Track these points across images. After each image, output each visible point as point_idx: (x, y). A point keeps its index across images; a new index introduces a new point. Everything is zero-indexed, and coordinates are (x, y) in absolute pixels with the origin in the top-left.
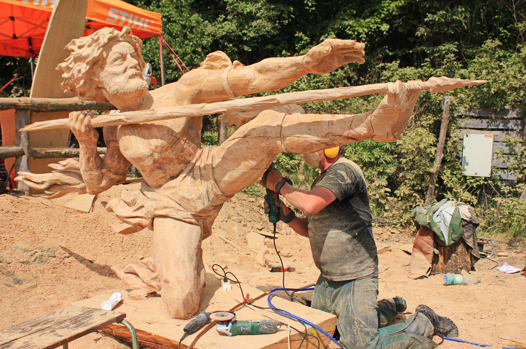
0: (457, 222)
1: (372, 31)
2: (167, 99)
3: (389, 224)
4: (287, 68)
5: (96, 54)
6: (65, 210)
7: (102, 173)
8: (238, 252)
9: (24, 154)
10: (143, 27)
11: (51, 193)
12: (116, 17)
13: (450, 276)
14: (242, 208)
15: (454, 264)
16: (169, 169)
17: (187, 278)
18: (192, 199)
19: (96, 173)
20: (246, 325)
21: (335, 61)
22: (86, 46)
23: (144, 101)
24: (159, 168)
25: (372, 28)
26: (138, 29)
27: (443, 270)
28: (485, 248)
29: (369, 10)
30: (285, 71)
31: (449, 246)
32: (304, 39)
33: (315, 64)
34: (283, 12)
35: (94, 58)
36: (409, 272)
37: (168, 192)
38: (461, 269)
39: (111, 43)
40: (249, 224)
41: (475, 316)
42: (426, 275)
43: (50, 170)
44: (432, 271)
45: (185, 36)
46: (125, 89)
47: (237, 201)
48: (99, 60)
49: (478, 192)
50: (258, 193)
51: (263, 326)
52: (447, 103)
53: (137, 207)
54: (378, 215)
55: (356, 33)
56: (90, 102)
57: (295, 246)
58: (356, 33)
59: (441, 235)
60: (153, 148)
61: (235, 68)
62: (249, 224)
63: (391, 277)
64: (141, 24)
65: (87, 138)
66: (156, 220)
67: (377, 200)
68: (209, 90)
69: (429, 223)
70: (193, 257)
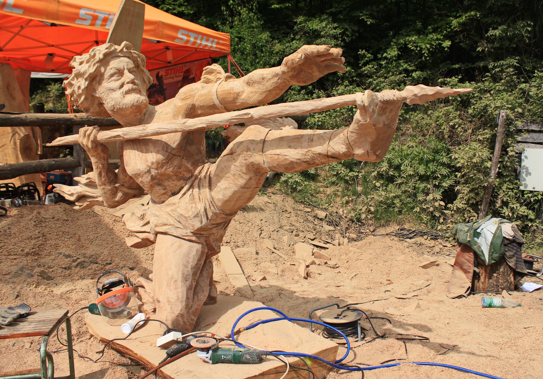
0: (499, 241)
1: (433, 48)
2: (166, 114)
3: (442, 237)
4: (270, 79)
5: (92, 70)
6: (113, 219)
7: (115, 187)
8: (284, 262)
9: (80, 165)
10: (211, 47)
11: (81, 204)
12: (185, 38)
13: (490, 298)
14: (296, 219)
15: (495, 284)
16: (169, 185)
17: (178, 299)
18: (189, 217)
19: (109, 187)
20: (228, 353)
21: (314, 70)
22: (85, 62)
23: (146, 116)
24: (159, 184)
25: (433, 45)
26: (201, 47)
27: (484, 289)
28: (536, 266)
29: (433, 26)
30: (269, 83)
31: (489, 265)
32: (368, 56)
33: (291, 74)
34: (346, 30)
35: (90, 74)
36: (448, 291)
37: (169, 209)
38: (503, 289)
39: (108, 58)
40: (301, 234)
41: (503, 346)
42: (464, 295)
43: (76, 183)
44: (472, 290)
45: (255, 55)
46: (121, 104)
47: (292, 211)
48: (97, 76)
49: (536, 206)
50: (315, 204)
51: (245, 356)
52: (502, 117)
53: (145, 223)
54: (432, 228)
55: (418, 49)
56: (94, 118)
57: (343, 257)
58: (418, 49)
59: (481, 254)
60: (150, 164)
61: (226, 81)
62: (301, 234)
63: (430, 294)
64: (209, 44)
65: (96, 153)
66: (158, 235)
67: (432, 213)
68: (201, 105)
69: (469, 241)
70: (188, 277)
